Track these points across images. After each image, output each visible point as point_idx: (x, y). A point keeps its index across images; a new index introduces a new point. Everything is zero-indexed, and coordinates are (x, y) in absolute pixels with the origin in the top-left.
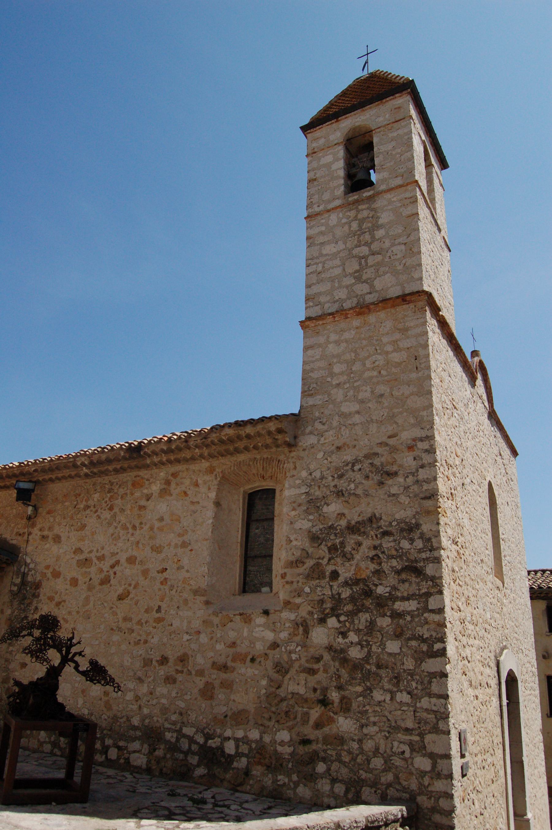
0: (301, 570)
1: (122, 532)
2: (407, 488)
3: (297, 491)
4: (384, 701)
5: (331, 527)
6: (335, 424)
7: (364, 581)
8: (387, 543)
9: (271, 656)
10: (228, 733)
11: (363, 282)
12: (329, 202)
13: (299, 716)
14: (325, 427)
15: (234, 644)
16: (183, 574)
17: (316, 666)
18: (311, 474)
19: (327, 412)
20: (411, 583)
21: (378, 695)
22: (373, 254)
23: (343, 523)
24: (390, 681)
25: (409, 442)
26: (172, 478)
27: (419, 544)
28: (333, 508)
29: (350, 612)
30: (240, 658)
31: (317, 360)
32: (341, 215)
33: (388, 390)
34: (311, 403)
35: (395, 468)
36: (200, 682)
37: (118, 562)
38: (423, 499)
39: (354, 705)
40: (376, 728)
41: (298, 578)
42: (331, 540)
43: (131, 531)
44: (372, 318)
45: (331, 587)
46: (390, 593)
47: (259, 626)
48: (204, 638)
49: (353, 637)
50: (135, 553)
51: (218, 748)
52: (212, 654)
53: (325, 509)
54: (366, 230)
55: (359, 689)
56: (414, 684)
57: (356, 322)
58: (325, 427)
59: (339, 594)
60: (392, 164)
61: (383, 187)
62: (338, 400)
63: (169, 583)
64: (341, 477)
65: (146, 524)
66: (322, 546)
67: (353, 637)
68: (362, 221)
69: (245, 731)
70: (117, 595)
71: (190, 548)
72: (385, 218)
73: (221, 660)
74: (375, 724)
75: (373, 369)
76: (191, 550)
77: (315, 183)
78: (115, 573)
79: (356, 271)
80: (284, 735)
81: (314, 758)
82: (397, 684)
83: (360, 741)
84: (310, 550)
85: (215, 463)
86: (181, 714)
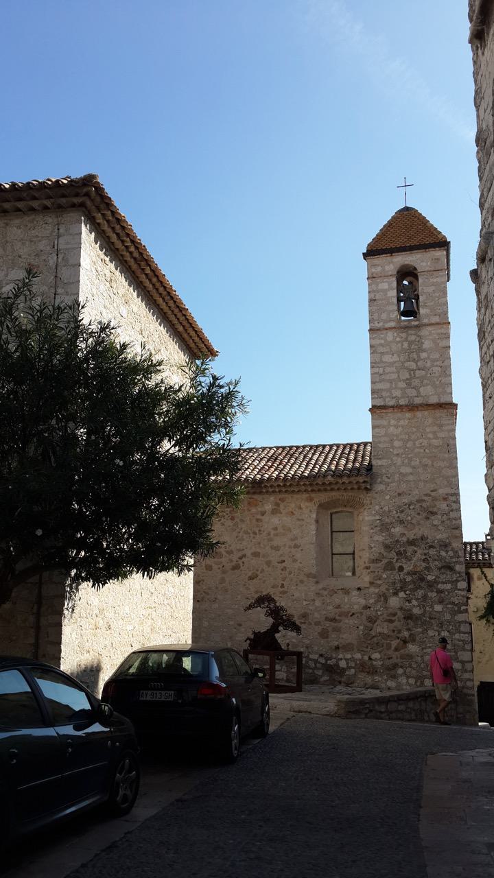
1: (245, 536)
2: (443, 522)
3: (373, 518)
5: (397, 541)
6: (397, 479)
7: (419, 572)
8: (432, 552)
9: (364, 614)
10: (341, 656)
12: (386, 321)
13: (385, 645)
14: (390, 480)
15: (339, 607)
16: (297, 565)
17: (393, 618)
18: (382, 508)
19: (391, 471)
20: (447, 575)
21: (431, 633)
22: (419, 370)
23: (405, 539)
25: (444, 495)
26: (280, 502)
27: (451, 553)
28: (397, 530)
30: (345, 614)
31: (382, 436)
33: (430, 463)
34: (380, 464)
35: (435, 510)
36: (319, 629)
37: (244, 556)
38: (453, 529)
39: (417, 639)
40: (430, 650)
41: (378, 570)
43: (252, 535)
44: (419, 414)
45: (400, 575)
46: (435, 579)
47: (355, 596)
48: (318, 603)
49: (414, 602)
50: (258, 550)
51: (335, 665)
52: (325, 612)
53: (392, 530)
55: (420, 630)
56: (451, 627)
57: (408, 415)
58: (390, 480)
59: (405, 579)
60: (432, 304)
61: (426, 321)
62: (398, 464)
63: (288, 570)
64: (402, 512)
65: (264, 532)
66: (392, 552)
67: (414, 602)
68: (411, 343)
69: (351, 654)
70: (247, 577)
71: (300, 548)
72: (427, 344)
73: (331, 616)
74: (430, 647)
75: (420, 447)
76: (302, 550)
77: (375, 303)
78: (243, 563)
79: (407, 379)
80: (376, 656)
81: (395, 666)
83: (422, 656)
85: (313, 495)
86: (307, 647)
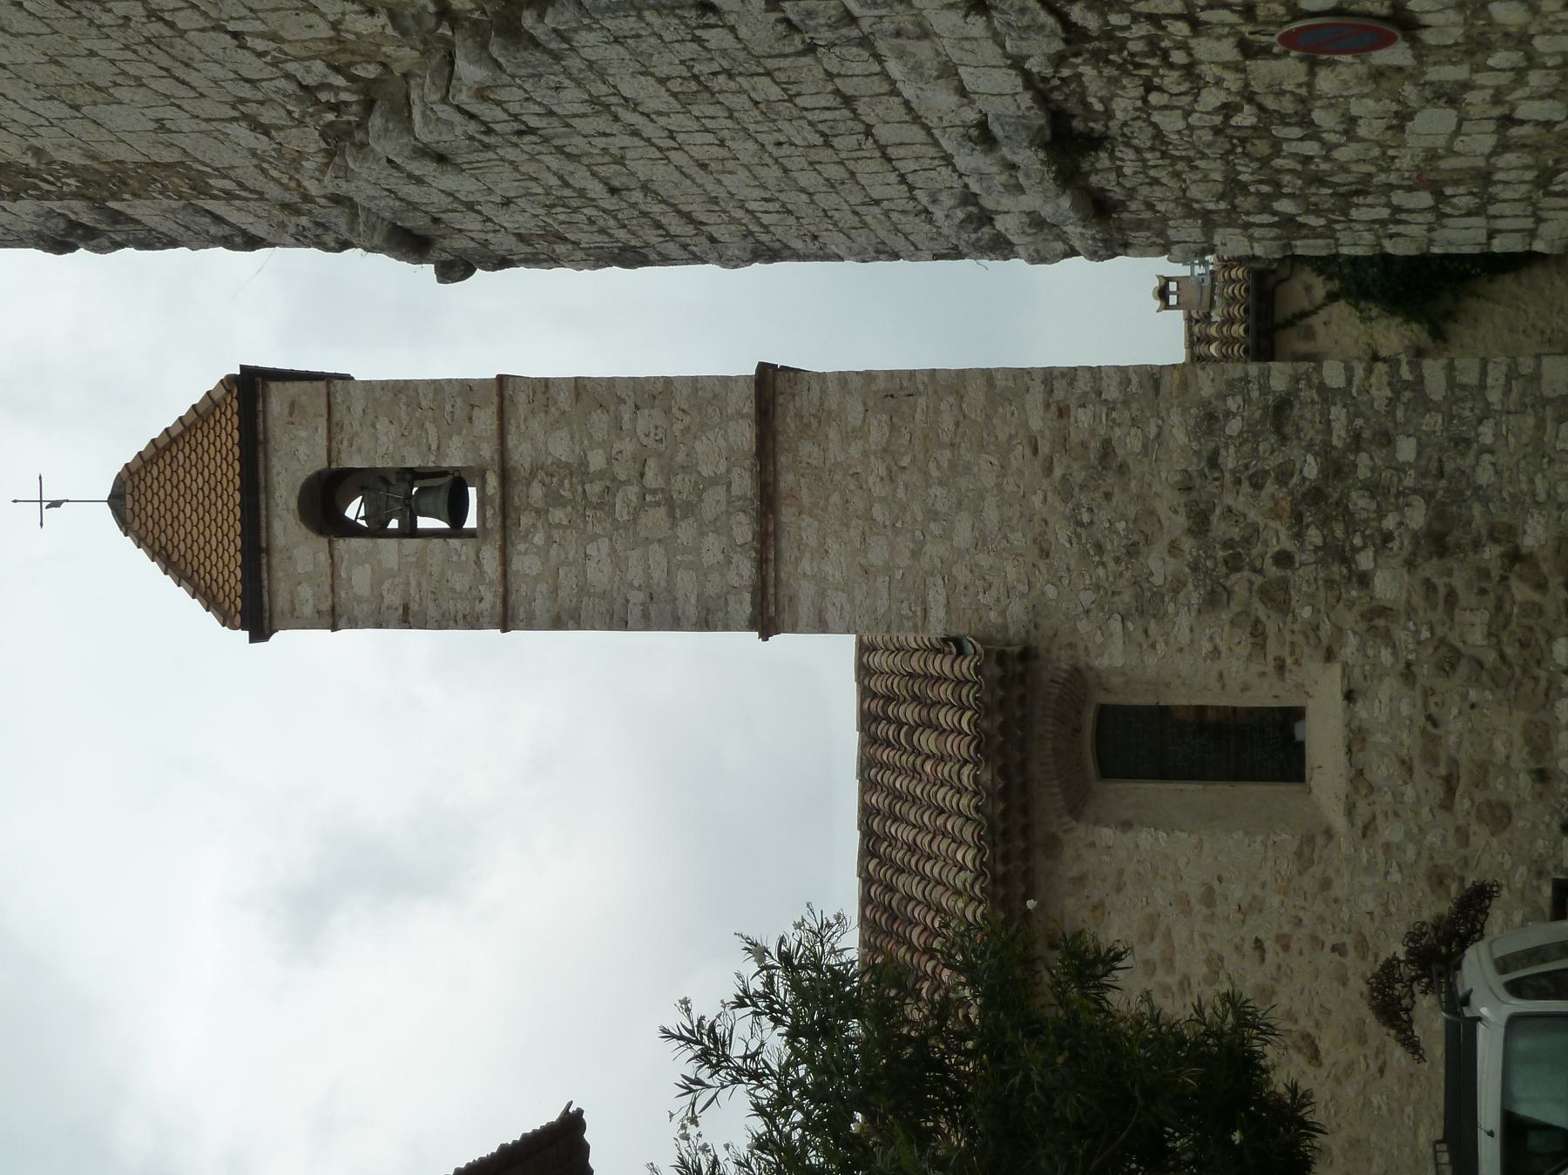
0: (1271, 628)
4: (1493, 464)
5: (1195, 568)
8: (1229, 460)
11: (701, 500)
15: (1407, 766)
17: (1442, 591)
23: (1188, 544)
24: (1463, 455)
27: (1232, 404)
28: (1160, 567)
29: (1347, 528)
32: (522, 547)
36: (1480, 835)
39: (1505, 518)
40: (1538, 479)
42: (1224, 565)
46: (1316, 455)
54: (580, 489)
55: (1477, 510)
59: (1317, 549)
64: (1099, 548)
66: (1229, 584)
67: (1390, 522)
73: (1438, 789)
74: (1531, 481)
76: (1220, 880)
82: (1468, 442)
84: (1235, 608)
